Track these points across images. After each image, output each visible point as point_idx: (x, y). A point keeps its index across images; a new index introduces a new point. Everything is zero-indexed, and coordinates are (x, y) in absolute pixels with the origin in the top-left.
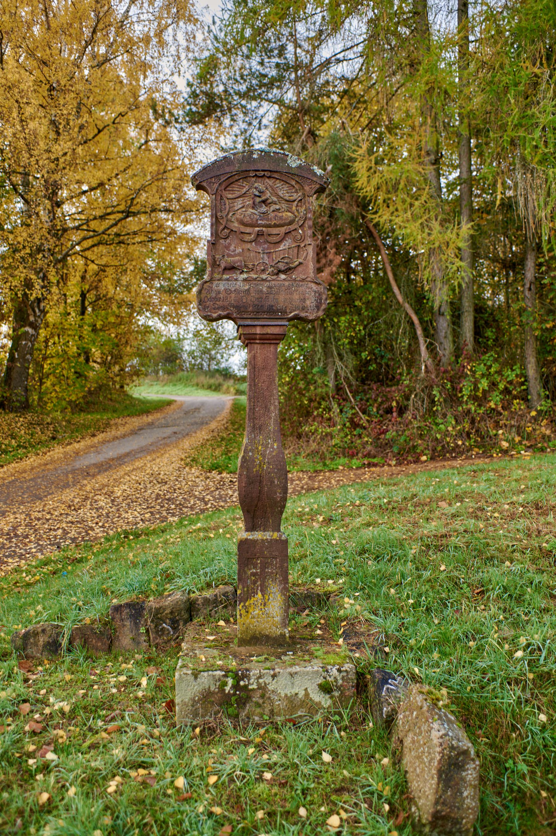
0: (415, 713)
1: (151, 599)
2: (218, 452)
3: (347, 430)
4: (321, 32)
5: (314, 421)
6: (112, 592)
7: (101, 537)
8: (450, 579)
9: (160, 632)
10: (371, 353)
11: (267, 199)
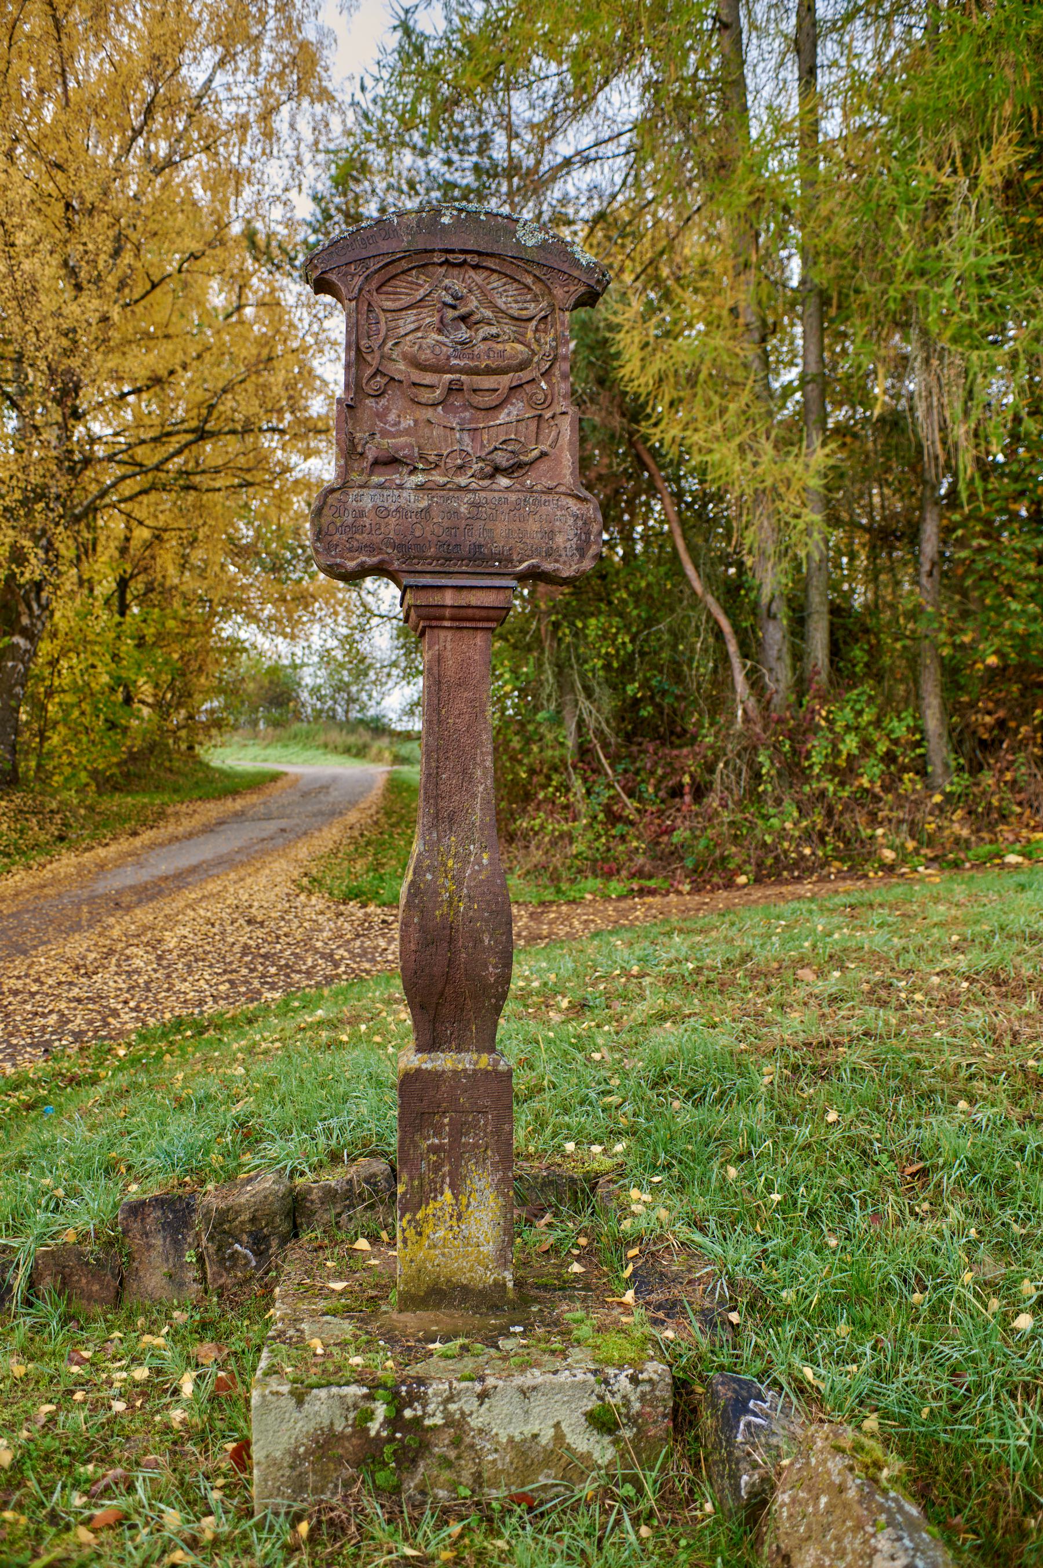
0: (824, 1500)
1: (210, 1187)
2: (359, 866)
3: (598, 827)
5: (538, 809)
6: (129, 1168)
7: (131, 1031)
8: (852, 1142)
9: (228, 1262)
10: (645, 684)
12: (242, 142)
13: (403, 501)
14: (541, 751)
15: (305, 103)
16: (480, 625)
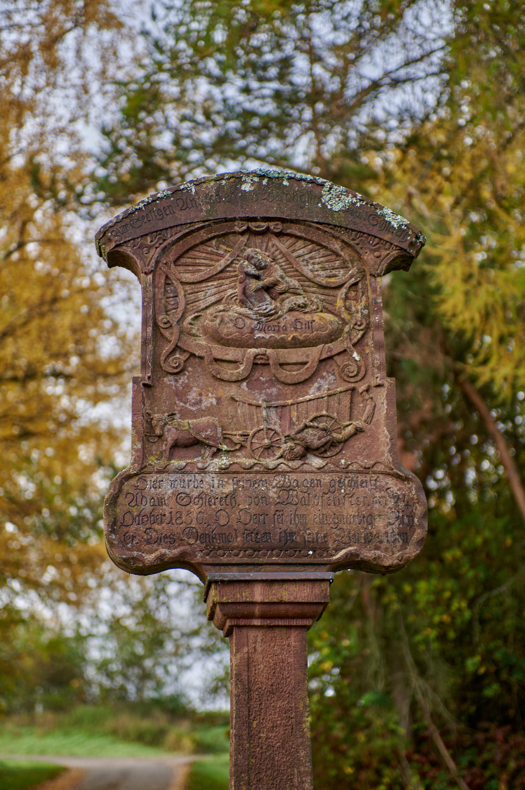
4: (359, 35)
11: (275, 284)
12: (24, 72)
13: (205, 486)
14: (370, 739)
15: (92, 30)
16: (294, 622)
